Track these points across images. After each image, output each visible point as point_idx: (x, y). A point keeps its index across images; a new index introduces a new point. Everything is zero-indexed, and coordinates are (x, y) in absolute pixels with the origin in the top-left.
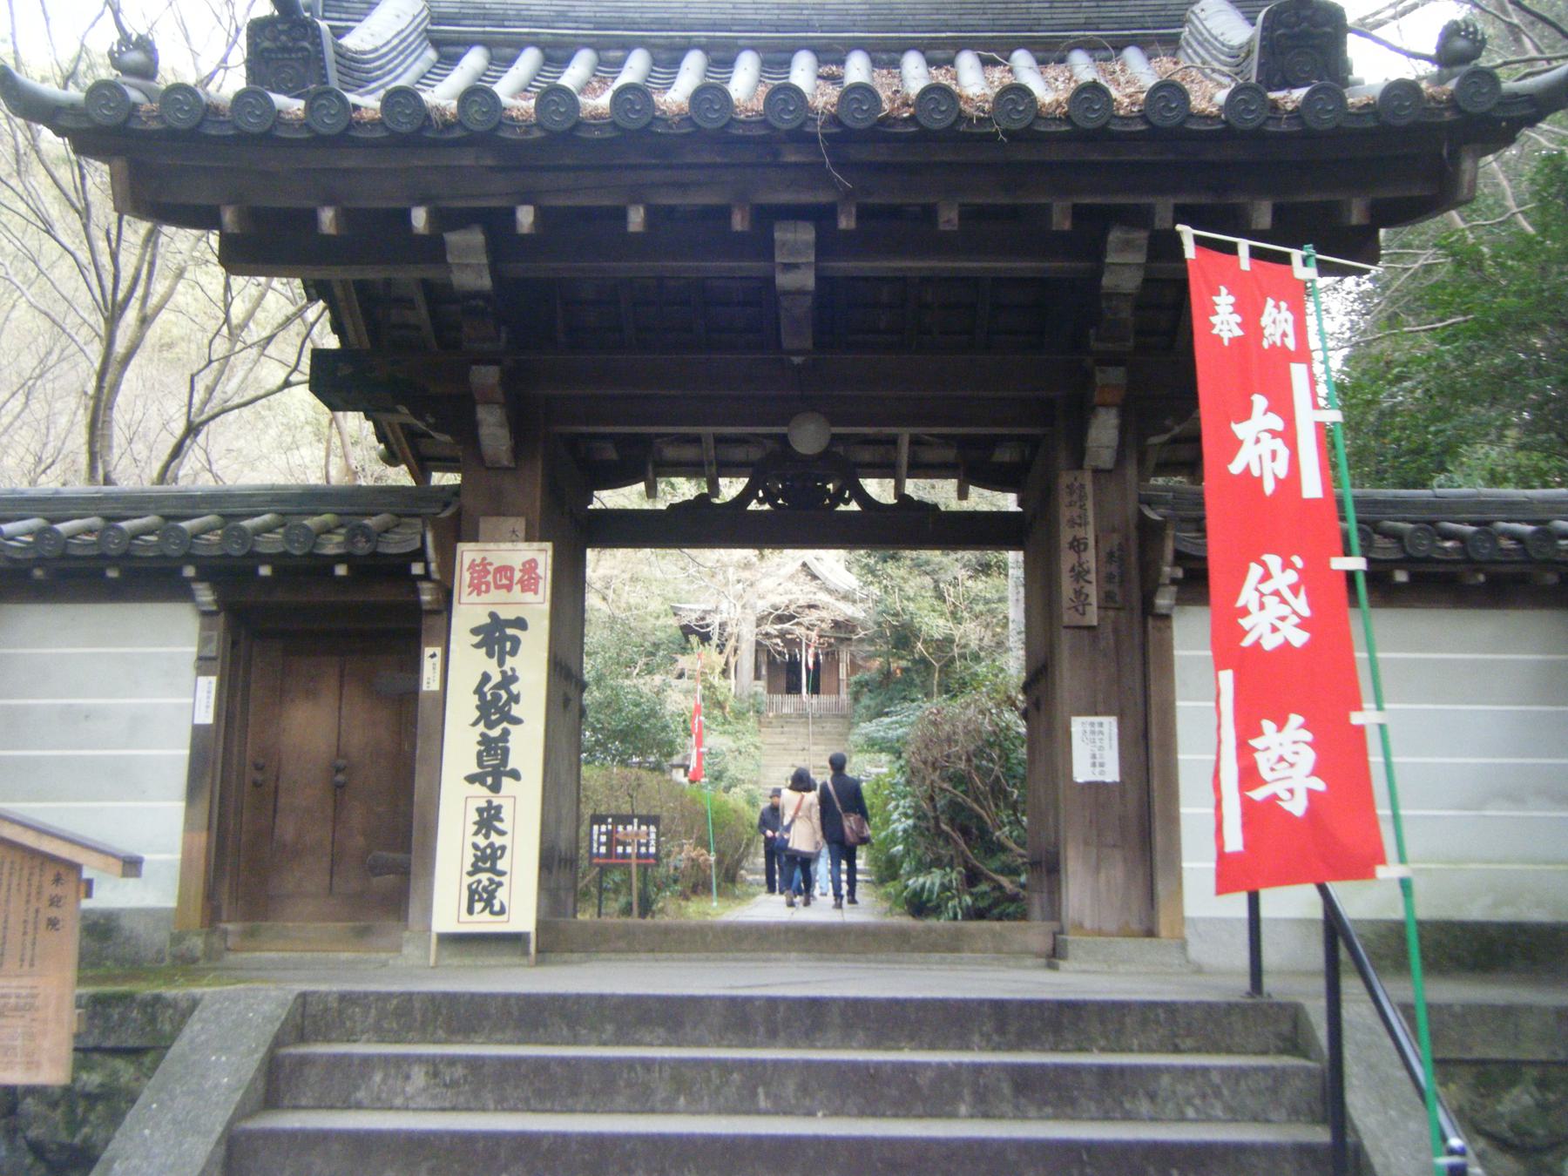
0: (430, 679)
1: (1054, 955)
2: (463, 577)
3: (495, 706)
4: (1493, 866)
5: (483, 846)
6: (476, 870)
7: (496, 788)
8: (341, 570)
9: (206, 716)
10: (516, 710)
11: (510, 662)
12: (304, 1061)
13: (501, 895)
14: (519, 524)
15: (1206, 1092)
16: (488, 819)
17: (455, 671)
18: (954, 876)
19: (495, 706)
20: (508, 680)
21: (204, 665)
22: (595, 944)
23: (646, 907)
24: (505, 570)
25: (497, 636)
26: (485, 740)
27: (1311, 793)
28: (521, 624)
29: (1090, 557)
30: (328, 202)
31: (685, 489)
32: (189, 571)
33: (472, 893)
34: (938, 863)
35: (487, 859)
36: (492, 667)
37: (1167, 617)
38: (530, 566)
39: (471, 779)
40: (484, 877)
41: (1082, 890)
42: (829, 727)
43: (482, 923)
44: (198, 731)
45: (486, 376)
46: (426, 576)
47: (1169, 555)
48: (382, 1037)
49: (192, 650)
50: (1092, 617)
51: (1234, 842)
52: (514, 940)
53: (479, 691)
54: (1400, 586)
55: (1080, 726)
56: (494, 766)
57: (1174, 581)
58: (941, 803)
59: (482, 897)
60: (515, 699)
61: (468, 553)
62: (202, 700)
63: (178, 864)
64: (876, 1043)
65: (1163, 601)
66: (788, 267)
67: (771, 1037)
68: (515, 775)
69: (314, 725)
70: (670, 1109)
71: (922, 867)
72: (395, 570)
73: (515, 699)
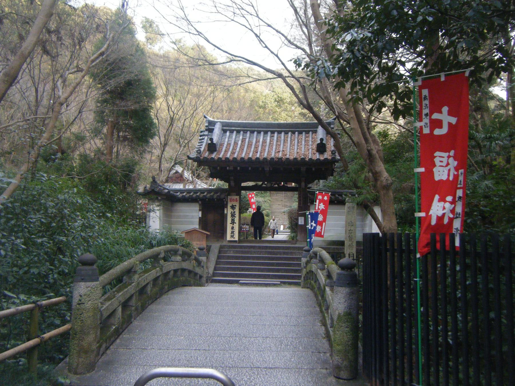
0: (225, 212)
2: (229, 200)
3: (233, 215)
5: (232, 232)
9: (200, 216)
16: (233, 228)
17: (229, 211)
19: (233, 215)
20: (234, 212)
21: (200, 210)
23: (247, 238)
25: (233, 207)
27: (450, 124)
30: (239, 166)
35: (233, 232)
37: (309, 206)
38: (236, 199)
43: (232, 239)
44: (200, 218)
50: (302, 205)
51: (324, 223)
52: (235, 241)
54: (438, 349)
56: (233, 222)
59: (232, 236)
61: (229, 197)
62: (200, 214)
63: (328, 214)
65: (309, 204)
69: (211, 217)
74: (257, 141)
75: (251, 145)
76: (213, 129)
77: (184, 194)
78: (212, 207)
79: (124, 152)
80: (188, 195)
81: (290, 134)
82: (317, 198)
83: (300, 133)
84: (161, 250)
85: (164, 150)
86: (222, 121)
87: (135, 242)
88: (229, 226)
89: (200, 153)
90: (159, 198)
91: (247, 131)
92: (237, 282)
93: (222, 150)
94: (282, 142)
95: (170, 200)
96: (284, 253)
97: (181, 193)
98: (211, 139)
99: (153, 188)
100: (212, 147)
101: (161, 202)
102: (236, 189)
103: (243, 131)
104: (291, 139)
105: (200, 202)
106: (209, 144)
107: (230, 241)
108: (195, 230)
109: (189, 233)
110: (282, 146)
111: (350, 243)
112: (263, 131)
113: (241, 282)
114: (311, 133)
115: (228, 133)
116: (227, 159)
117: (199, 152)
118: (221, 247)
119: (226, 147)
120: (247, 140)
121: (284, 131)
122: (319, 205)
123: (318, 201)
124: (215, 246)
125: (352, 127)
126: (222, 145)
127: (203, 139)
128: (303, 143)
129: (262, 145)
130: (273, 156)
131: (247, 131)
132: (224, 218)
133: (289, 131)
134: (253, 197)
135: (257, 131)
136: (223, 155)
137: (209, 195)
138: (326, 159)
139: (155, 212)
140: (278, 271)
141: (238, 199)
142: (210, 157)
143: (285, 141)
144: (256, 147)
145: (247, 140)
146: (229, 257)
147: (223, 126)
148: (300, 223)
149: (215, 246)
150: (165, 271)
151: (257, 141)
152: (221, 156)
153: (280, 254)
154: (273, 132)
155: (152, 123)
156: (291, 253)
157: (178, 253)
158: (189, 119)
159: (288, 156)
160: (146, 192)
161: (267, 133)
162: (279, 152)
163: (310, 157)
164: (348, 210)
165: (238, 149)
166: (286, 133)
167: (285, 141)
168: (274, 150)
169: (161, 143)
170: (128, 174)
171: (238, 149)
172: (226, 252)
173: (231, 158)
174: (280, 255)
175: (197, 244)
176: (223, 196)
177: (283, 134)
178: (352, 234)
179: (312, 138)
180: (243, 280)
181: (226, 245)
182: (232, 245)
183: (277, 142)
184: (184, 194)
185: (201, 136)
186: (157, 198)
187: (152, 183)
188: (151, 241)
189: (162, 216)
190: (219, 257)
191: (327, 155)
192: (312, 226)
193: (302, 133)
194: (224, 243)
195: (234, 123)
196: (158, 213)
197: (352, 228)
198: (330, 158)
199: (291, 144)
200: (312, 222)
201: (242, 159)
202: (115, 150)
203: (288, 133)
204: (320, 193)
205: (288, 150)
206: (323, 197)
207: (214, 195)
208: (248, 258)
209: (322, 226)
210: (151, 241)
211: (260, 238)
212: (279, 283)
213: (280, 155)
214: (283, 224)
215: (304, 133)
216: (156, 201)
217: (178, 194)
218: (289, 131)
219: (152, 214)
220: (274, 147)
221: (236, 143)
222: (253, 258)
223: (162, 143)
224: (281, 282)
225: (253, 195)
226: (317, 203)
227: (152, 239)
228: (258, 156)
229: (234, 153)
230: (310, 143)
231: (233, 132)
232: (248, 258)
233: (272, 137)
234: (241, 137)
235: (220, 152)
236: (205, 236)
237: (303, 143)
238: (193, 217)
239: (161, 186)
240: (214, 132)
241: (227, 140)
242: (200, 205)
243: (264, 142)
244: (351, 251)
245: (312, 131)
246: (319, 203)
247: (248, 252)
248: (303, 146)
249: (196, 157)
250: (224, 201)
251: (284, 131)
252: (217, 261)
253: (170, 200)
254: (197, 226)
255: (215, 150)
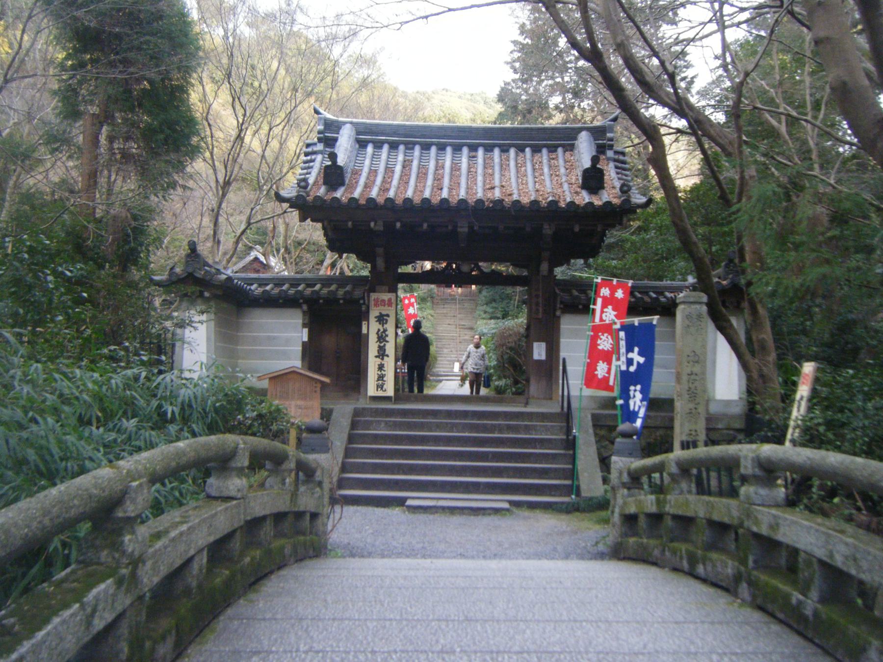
1: (526, 404)
2: (372, 303)
4: (561, 368)
5: (382, 374)
6: (378, 380)
7: (383, 359)
8: (341, 302)
9: (306, 339)
10: (387, 339)
11: (385, 326)
12: (359, 421)
13: (385, 387)
14: (387, 288)
15: (547, 430)
16: (381, 367)
17: (371, 328)
18: (509, 382)
20: (385, 331)
22: (407, 400)
24: (383, 301)
25: (382, 319)
26: (379, 347)
28: (388, 315)
29: (540, 300)
30: (398, 220)
31: (428, 265)
32: (301, 301)
33: (378, 386)
34: (505, 377)
35: (381, 377)
36: (380, 327)
37: (559, 318)
38: (390, 300)
39: (376, 357)
40: (380, 382)
41: (534, 388)
42: (466, 305)
43: (380, 393)
44: (303, 343)
45: (380, 251)
46: (364, 303)
47: (559, 302)
48: (371, 416)
49: (301, 321)
52: (387, 399)
53: (377, 333)
55: (535, 345)
56: (382, 353)
57: (560, 308)
58: (506, 357)
59: (380, 387)
60: (387, 336)
61: (373, 296)
64: (479, 419)
65: (558, 313)
66: (462, 227)
67: (456, 418)
68: (388, 356)
69: (330, 341)
70: (436, 431)
71: (500, 378)
72: (356, 302)
73: (387, 336)
74: (439, 167)
75: (426, 174)
76: (336, 140)
77: (268, 288)
78: (335, 319)
79: (126, 185)
80: (276, 291)
81: (512, 151)
82: (597, 293)
83: (536, 150)
84: (132, 476)
85: (224, 195)
86: (355, 120)
87: (109, 410)
88: (373, 363)
89: (305, 187)
90: (207, 294)
91: (415, 143)
92: (400, 502)
93: (357, 182)
94: (497, 168)
95: (233, 301)
96: (510, 428)
97: (260, 285)
98: (333, 157)
99: (190, 270)
100: (334, 175)
101: (212, 303)
102: (387, 279)
103: (406, 144)
104: (517, 164)
105: (305, 307)
106: (327, 167)
107: (375, 399)
108: (294, 372)
109: (278, 378)
110: (497, 176)
111: (691, 406)
112: (451, 145)
113: (409, 502)
114: (560, 150)
115: (370, 149)
116: (371, 200)
117: (303, 183)
118: (357, 413)
119: (368, 178)
120: (415, 163)
121: (499, 146)
122: (602, 312)
123: (599, 301)
124: (343, 410)
125: (822, 34)
126: (357, 173)
127: (313, 161)
128: (546, 170)
129: (452, 175)
130: (480, 195)
131: (415, 143)
132: (359, 343)
133: (510, 146)
134: (412, 305)
135: (437, 144)
136: (362, 194)
137: (325, 291)
138: (608, 203)
139: (196, 329)
140: (498, 472)
141: (393, 300)
142: (328, 197)
143: (504, 167)
144: (438, 179)
145: (415, 163)
146: (376, 438)
147: (358, 133)
148: (536, 357)
149: (343, 410)
150: (150, 577)
151: (439, 167)
152: (356, 194)
153: (500, 429)
154: (473, 148)
155: (191, 122)
156: (527, 429)
157: (233, 464)
158: (281, 127)
159: (515, 197)
160: (174, 279)
161: (460, 150)
162: (493, 188)
163: (568, 200)
164: (687, 322)
165: (395, 182)
166: (504, 150)
167: (504, 167)
168: (480, 183)
169: (217, 181)
170: (131, 240)
171: (395, 182)
172: (368, 425)
173: (381, 200)
174: (500, 431)
175: (301, 410)
176: (357, 293)
177: (497, 151)
178: (697, 384)
179: (566, 161)
180: (416, 499)
181: (364, 409)
182: (381, 410)
183: (485, 168)
184: (268, 288)
185: (306, 154)
186: (201, 295)
187: (188, 256)
188: (160, 406)
189: (213, 336)
190: (351, 439)
191: (609, 195)
192: (630, 362)
193: (540, 151)
194: (362, 404)
195: (385, 125)
196: (203, 329)
197: (697, 369)
198: (616, 201)
199: (518, 172)
200: (629, 349)
201: (407, 201)
202: (102, 181)
203: (507, 151)
204: (606, 283)
205: (514, 184)
206: (613, 290)
207: (337, 290)
208: (423, 440)
209: (609, 364)
210: (160, 406)
211: (421, 390)
212: (506, 505)
213: (497, 194)
214: (458, 361)
215: (545, 151)
216: (199, 301)
217: (253, 287)
218: (510, 146)
219: (188, 333)
220: (480, 178)
221: (389, 170)
222: (437, 440)
223: (221, 180)
224: (511, 502)
225: (413, 300)
226: (598, 307)
227: (164, 398)
228: (445, 194)
229: (388, 190)
230: (562, 170)
231: (381, 147)
232: (423, 440)
233: (472, 158)
234: (401, 158)
235: (353, 187)
236: (319, 385)
237: (546, 170)
238: (288, 342)
239: (210, 266)
240: (338, 144)
241: (367, 162)
242: (304, 312)
243: (455, 168)
244: (693, 427)
245: (563, 146)
246: (604, 306)
247: (422, 426)
248: (547, 177)
249: (298, 197)
250: (360, 305)
251: (499, 146)
252: (347, 449)
253: (233, 301)
254: (296, 363)
255: (342, 184)
